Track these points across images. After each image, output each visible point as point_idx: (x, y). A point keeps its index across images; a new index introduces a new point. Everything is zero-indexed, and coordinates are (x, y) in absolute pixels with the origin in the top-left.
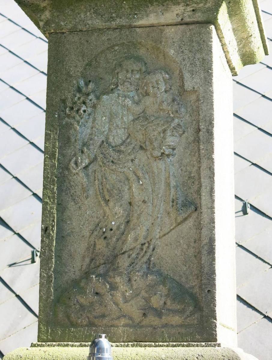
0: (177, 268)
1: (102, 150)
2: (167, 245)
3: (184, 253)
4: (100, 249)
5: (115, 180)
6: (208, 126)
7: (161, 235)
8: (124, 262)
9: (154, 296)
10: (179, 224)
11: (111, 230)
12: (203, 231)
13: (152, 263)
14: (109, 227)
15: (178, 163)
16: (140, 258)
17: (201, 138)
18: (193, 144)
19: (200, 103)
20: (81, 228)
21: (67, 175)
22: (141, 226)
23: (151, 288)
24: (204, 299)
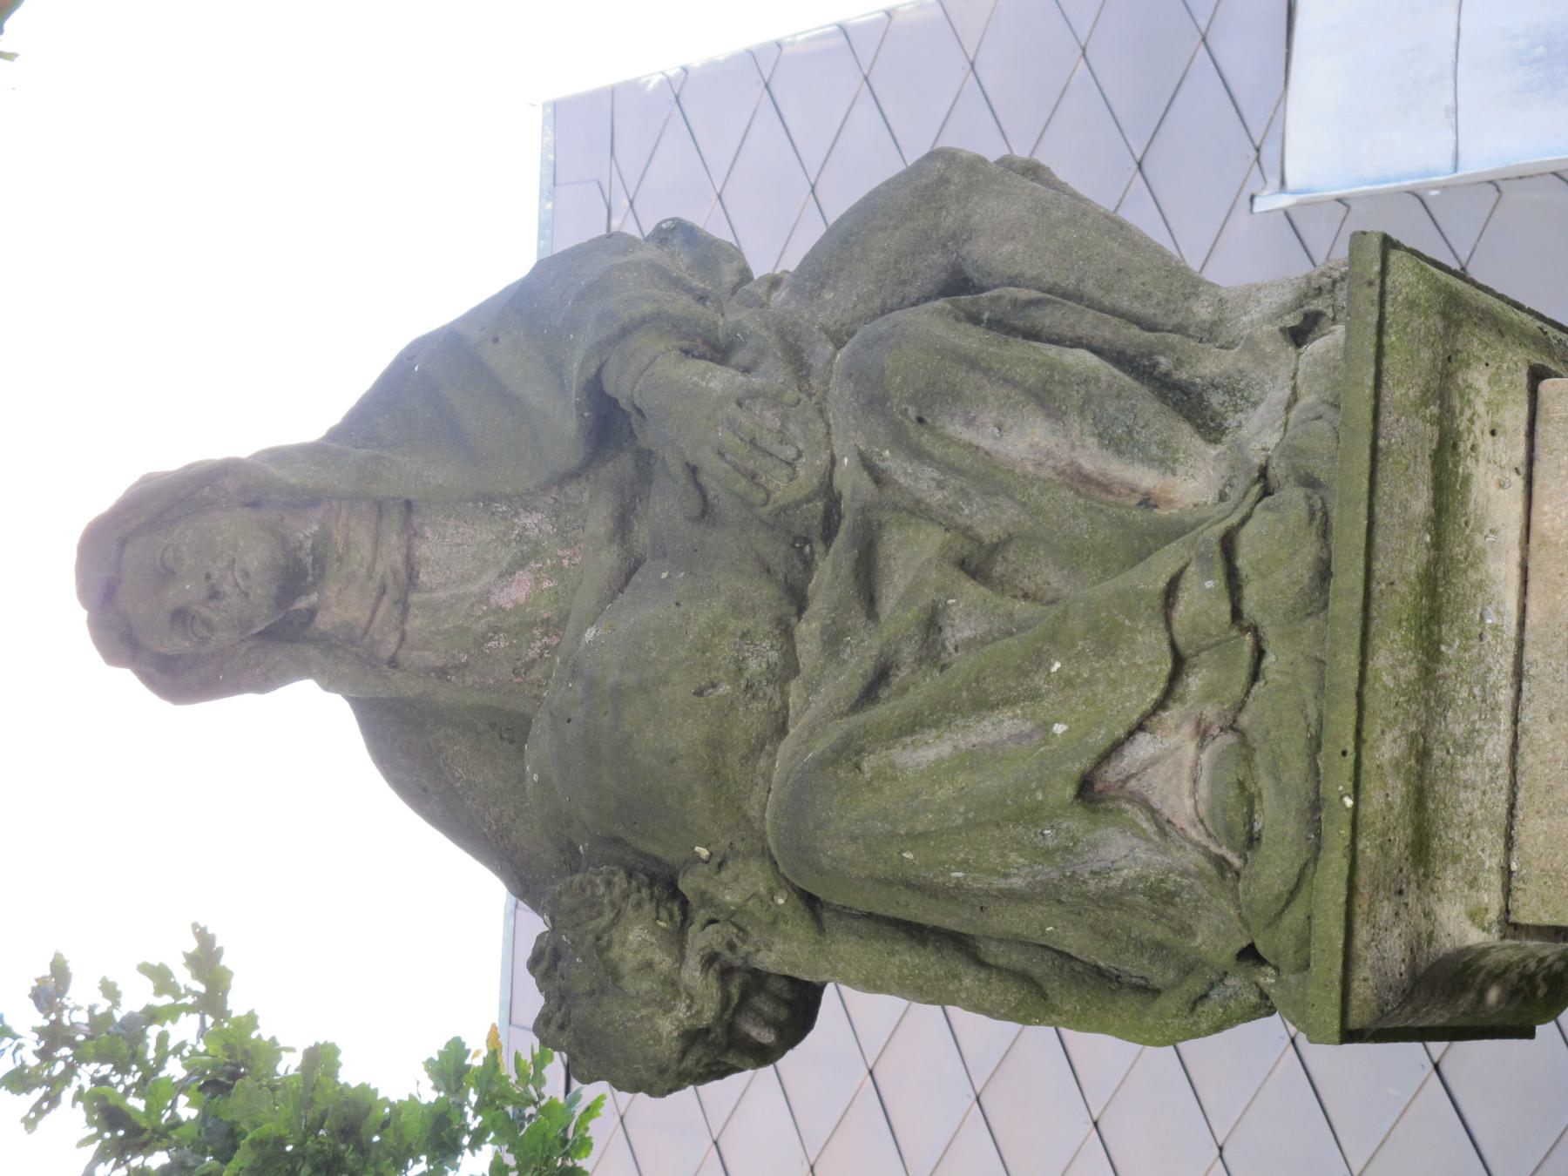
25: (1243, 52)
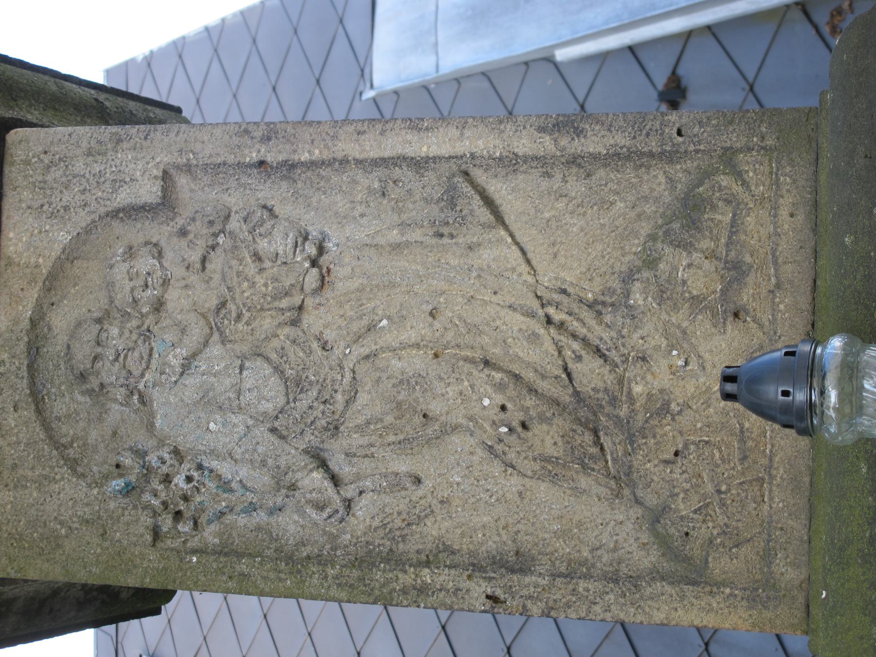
0: (617, 227)
1: (294, 432)
2: (555, 256)
3: (578, 206)
4: (555, 444)
5: (374, 394)
6: (252, 138)
7: (528, 269)
8: (591, 374)
9: (688, 287)
10: (499, 218)
11: (503, 408)
12: (520, 151)
13: (601, 298)
14: (494, 414)
15: (343, 226)
16: (584, 331)
17: (281, 158)
18: (300, 185)
19: (195, 162)
20: (498, 500)
21: (352, 536)
22: (498, 323)
23: (666, 293)
24: (702, 147)
25: (355, 25)
